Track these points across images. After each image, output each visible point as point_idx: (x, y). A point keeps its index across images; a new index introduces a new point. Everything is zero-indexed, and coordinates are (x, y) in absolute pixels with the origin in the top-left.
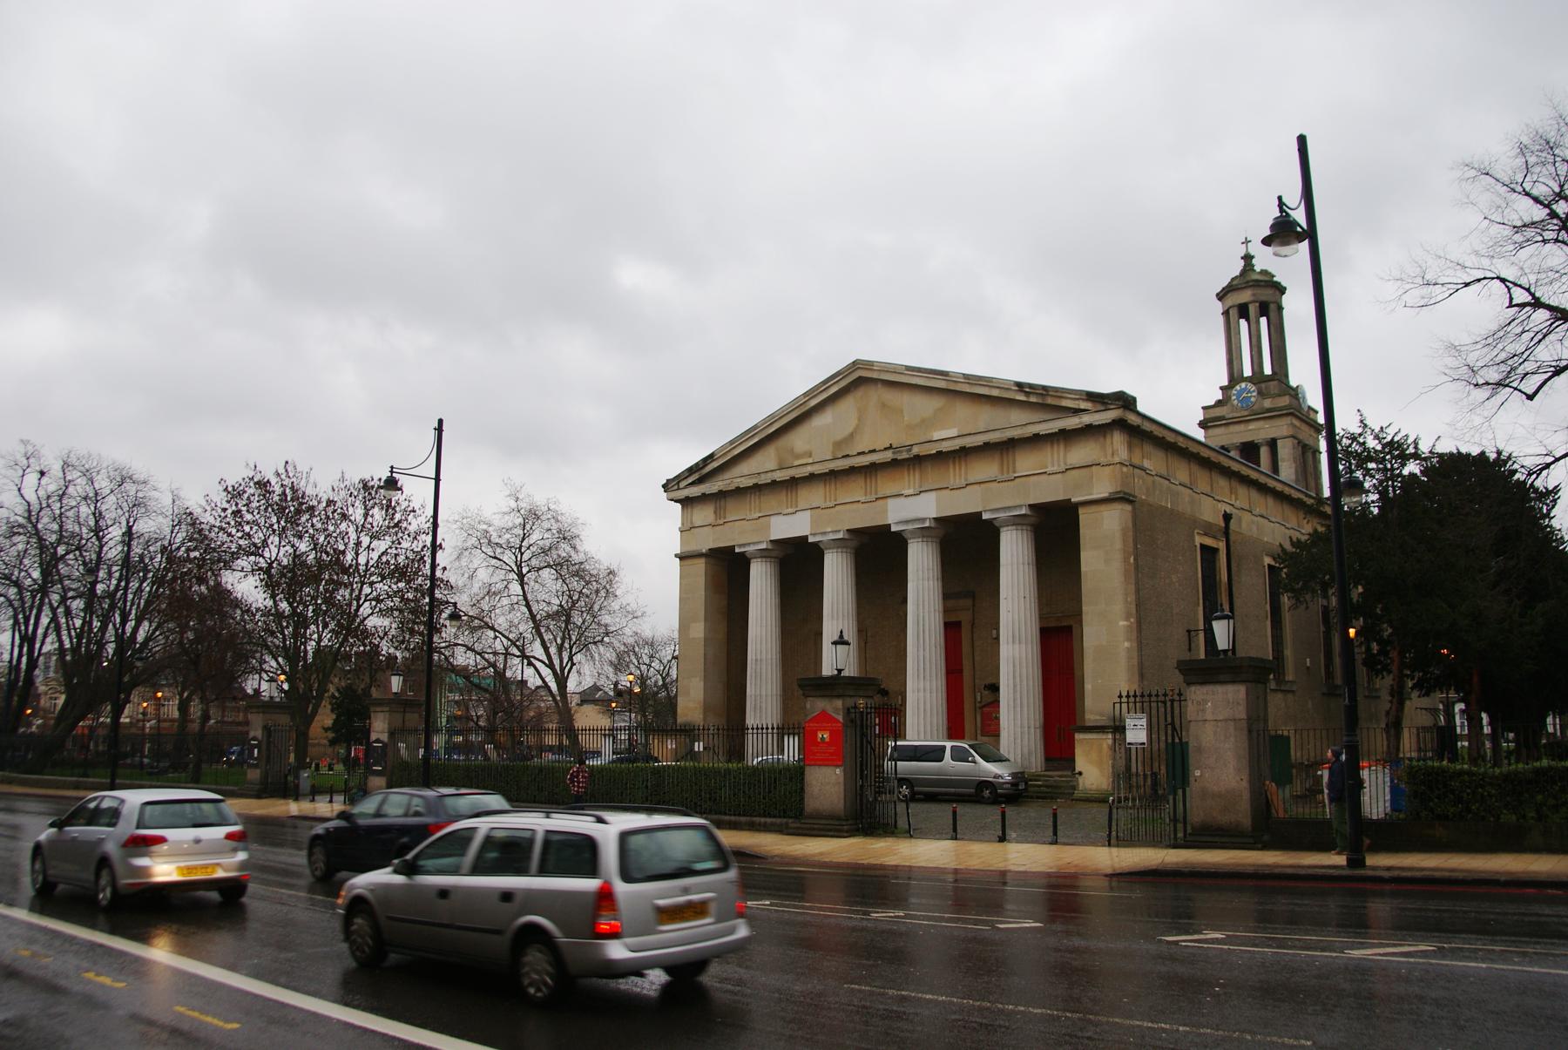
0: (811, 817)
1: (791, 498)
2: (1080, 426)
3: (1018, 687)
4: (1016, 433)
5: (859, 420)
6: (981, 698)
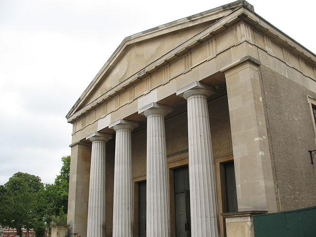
1: (167, 74)
4: (168, 57)
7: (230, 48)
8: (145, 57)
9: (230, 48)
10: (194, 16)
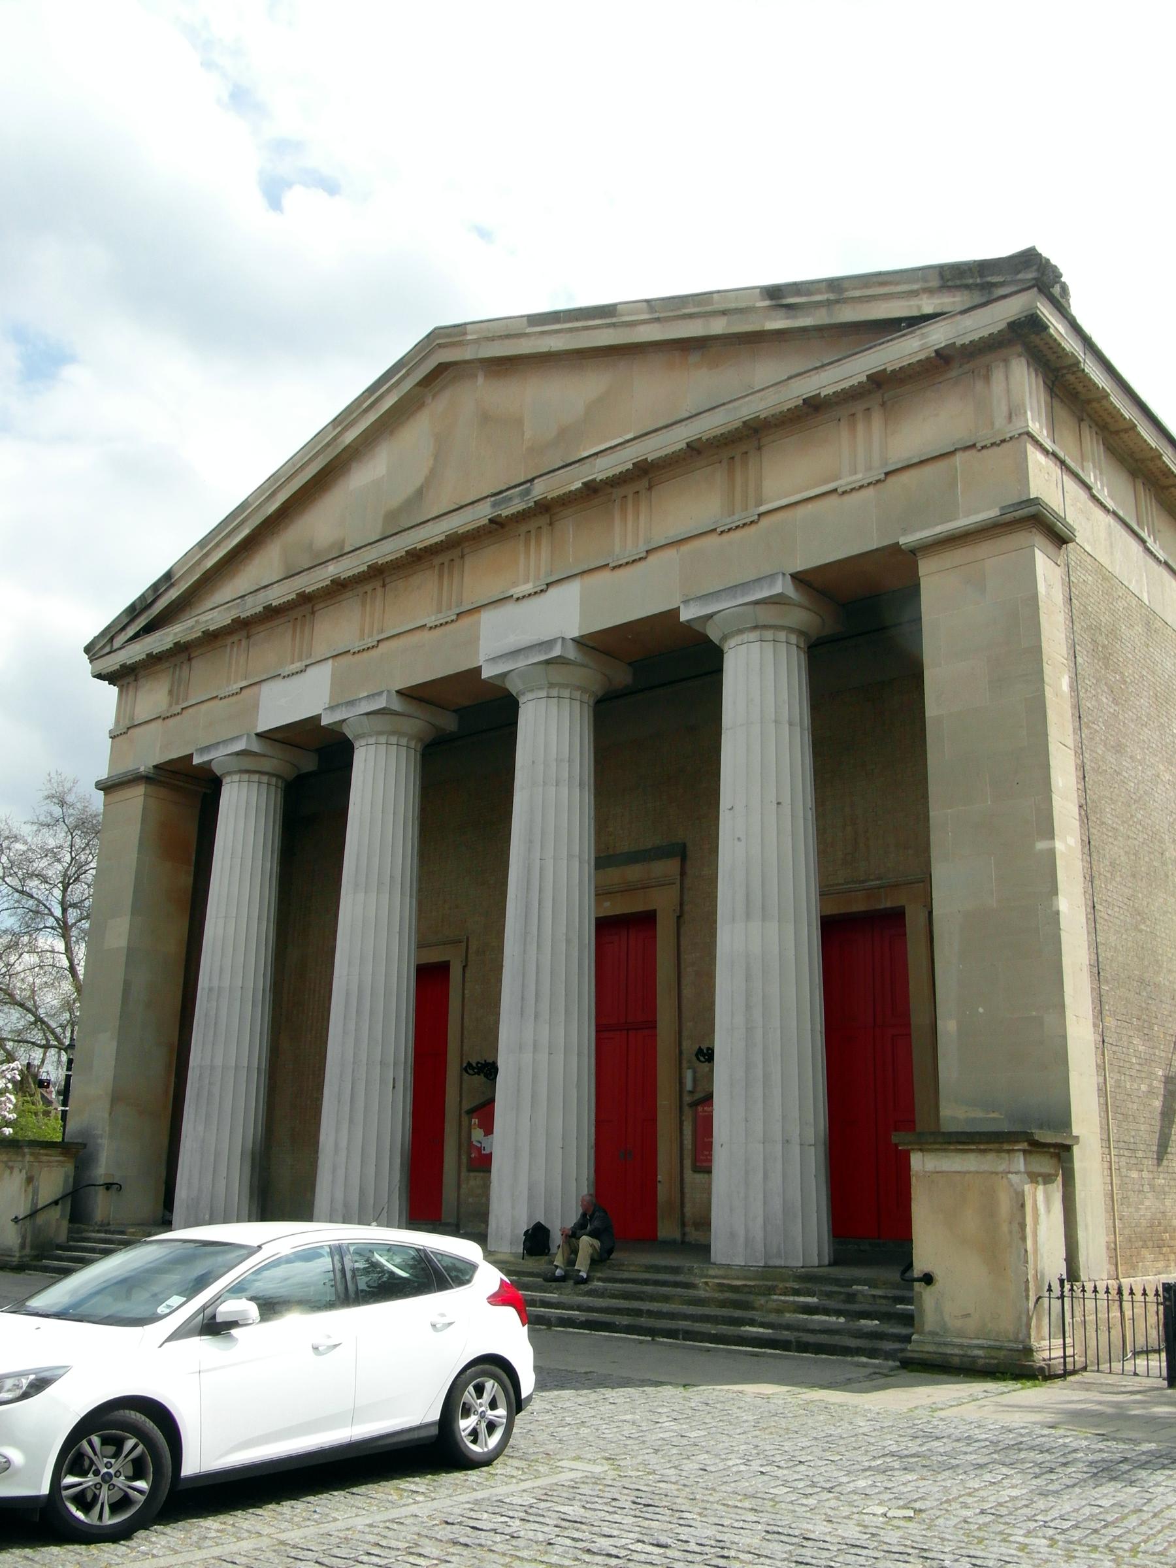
0: (712, 1264)
2: (922, 356)
3: (759, 1034)
5: (436, 457)
6: (695, 1080)
7: (952, 453)
8: (527, 436)
9: (952, 453)
10: (797, 288)
